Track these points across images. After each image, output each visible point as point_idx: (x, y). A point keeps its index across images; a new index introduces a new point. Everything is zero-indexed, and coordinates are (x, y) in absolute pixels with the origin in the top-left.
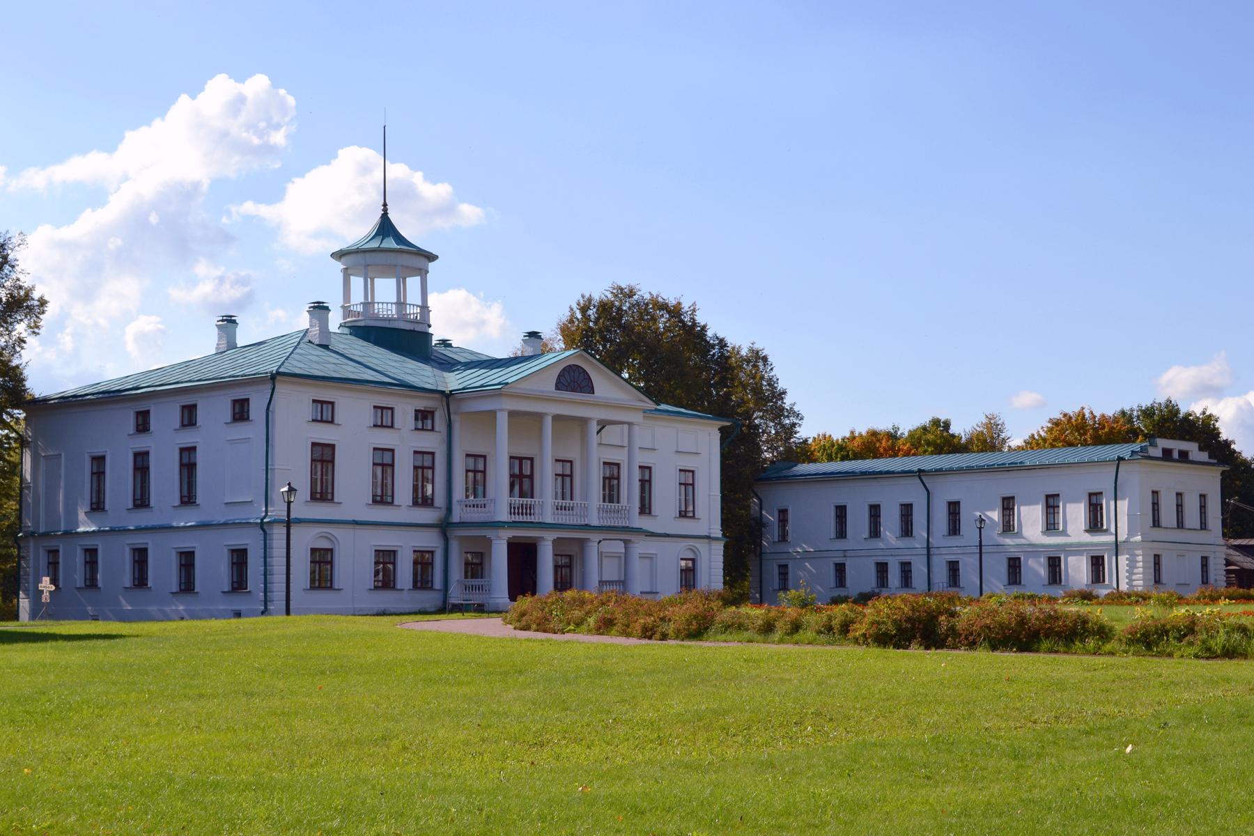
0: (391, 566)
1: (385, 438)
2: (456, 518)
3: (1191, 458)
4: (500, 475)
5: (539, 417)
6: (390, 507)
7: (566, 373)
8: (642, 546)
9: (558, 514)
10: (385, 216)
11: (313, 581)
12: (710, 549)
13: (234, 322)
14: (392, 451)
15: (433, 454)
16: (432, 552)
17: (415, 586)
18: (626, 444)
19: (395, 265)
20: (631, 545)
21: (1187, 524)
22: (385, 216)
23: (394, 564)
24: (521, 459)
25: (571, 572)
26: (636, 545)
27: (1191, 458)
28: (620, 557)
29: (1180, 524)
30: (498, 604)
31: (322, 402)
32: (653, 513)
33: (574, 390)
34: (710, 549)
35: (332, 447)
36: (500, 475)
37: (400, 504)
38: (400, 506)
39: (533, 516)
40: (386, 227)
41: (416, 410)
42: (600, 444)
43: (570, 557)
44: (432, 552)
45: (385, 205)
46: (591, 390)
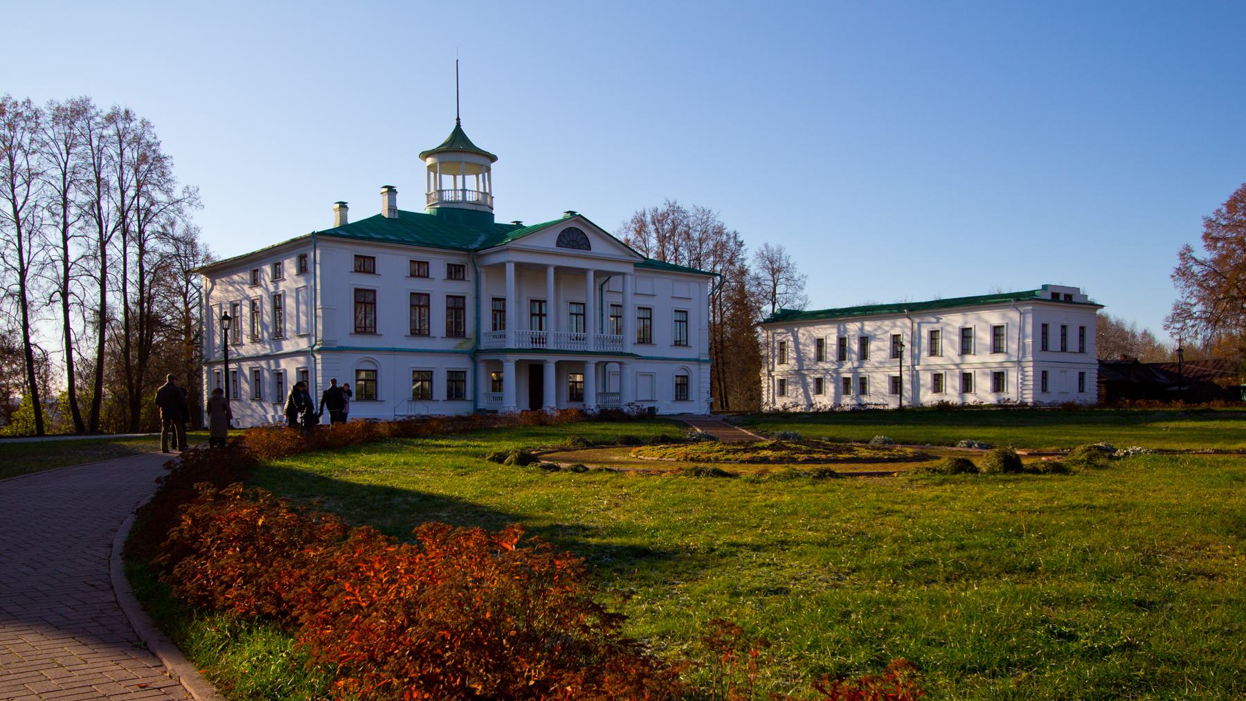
0: (426, 384)
1: (420, 286)
3: (1074, 300)
5: (544, 268)
7: (566, 234)
9: (570, 343)
10: (458, 125)
11: (676, 395)
12: (700, 369)
13: (346, 207)
14: (428, 295)
16: (465, 372)
20: (626, 366)
21: (1069, 348)
22: (458, 125)
23: (431, 381)
27: (1074, 300)
29: (1064, 349)
31: (419, 263)
32: (653, 342)
33: (573, 247)
34: (700, 369)
35: (374, 292)
40: (458, 134)
41: (448, 265)
45: (458, 119)
46: (589, 248)
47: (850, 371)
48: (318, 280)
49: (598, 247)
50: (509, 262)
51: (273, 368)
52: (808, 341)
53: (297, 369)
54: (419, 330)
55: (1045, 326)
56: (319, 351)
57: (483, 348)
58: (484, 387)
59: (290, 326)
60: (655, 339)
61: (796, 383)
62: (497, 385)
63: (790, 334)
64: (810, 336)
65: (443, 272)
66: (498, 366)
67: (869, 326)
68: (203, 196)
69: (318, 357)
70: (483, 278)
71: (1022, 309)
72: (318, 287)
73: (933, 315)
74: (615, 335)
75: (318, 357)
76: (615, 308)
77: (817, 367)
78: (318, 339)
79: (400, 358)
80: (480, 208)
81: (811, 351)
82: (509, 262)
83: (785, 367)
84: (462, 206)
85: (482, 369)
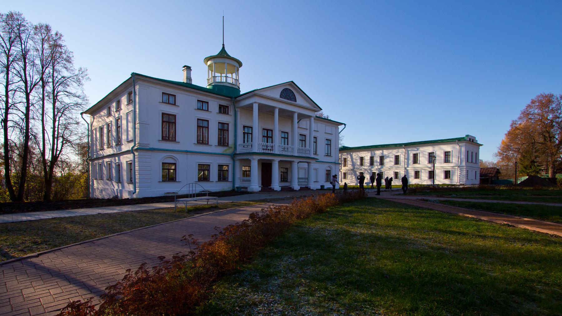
1: (203, 115)
2: (238, 151)
4: (257, 133)
6: (206, 146)
7: (285, 91)
8: (314, 165)
10: (223, 47)
14: (208, 121)
15: (228, 124)
17: (219, 180)
18: (308, 128)
19: (225, 63)
20: (310, 164)
22: (223, 47)
23: (209, 170)
24: (267, 130)
25: (287, 174)
26: (312, 164)
28: (305, 169)
29: (472, 162)
30: (253, 188)
33: (287, 99)
35: (175, 116)
36: (257, 133)
37: (212, 144)
38: (211, 145)
39: (273, 151)
41: (220, 105)
42: (299, 127)
43: (287, 168)
44: (228, 166)
45: (223, 45)
47: (377, 169)
48: (137, 106)
49: (300, 101)
50: (255, 102)
51: (117, 161)
52: (357, 158)
53: (127, 162)
54: (202, 141)
55: (468, 152)
56: (137, 150)
57: (238, 152)
58: (238, 174)
59: (124, 137)
60: (179, 177)
61: (352, 174)
62: (247, 174)
63: (349, 155)
64: (358, 156)
65: (217, 109)
66: (247, 162)
67: (386, 152)
68: (90, 73)
69: (136, 154)
70: (239, 114)
71: (460, 144)
72: (137, 110)
73: (415, 147)
74: (301, 147)
75: (136, 154)
76: (301, 136)
77: (361, 168)
78: (137, 143)
79: (190, 156)
80: (234, 86)
81: (358, 162)
82: (255, 102)
83: (346, 168)
84: (225, 84)
85: (238, 164)
